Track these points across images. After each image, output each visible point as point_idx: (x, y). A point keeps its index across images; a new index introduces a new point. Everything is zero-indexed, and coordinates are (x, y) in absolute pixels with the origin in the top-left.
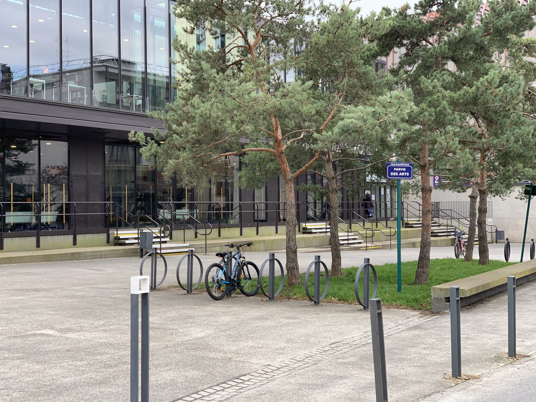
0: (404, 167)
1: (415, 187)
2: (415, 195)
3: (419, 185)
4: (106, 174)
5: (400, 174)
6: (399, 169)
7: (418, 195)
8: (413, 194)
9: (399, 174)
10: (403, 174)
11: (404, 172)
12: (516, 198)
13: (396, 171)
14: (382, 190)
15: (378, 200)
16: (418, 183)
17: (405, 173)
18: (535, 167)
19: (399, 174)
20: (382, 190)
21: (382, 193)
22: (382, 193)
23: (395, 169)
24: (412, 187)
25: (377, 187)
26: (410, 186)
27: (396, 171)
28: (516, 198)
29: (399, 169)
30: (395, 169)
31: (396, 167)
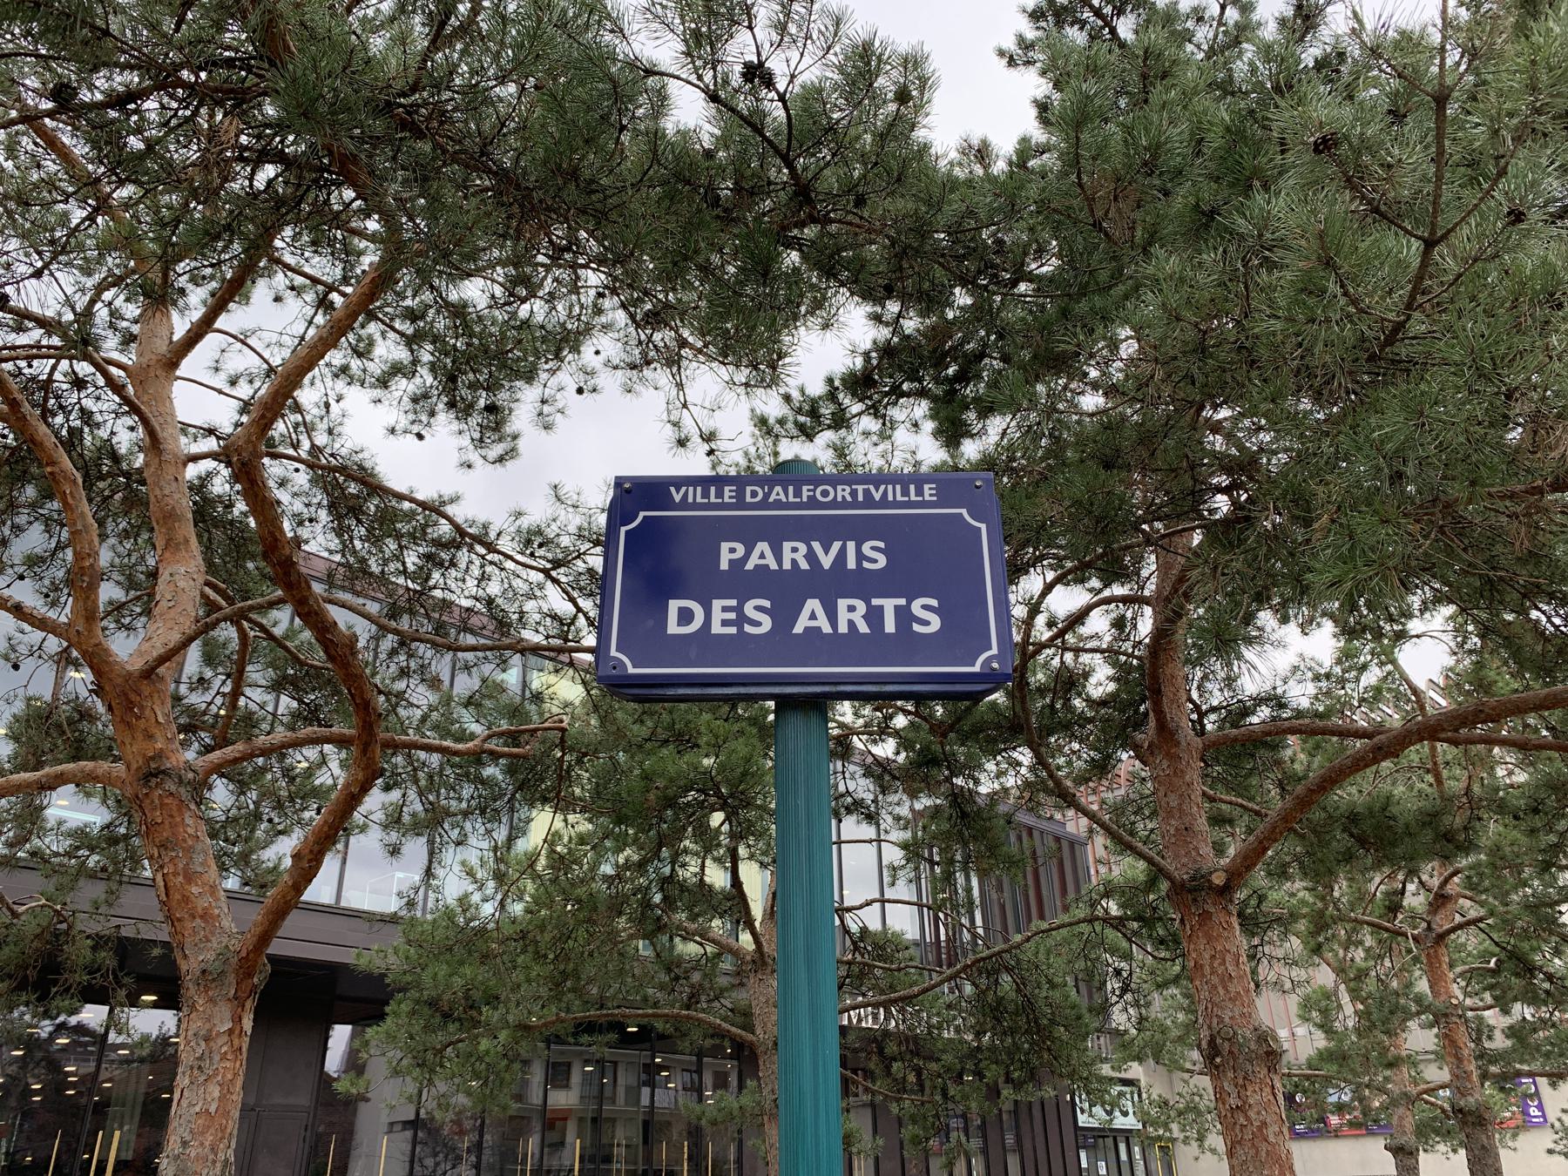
0: (859, 530)
1: (1191, 1116)
2: (1195, 1144)
3: (1202, 1107)
4: (856, 1164)
5: (811, 617)
6: (794, 554)
7: (1206, 1144)
8: (1186, 1141)
9: (784, 614)
10: (851, 613)
11: (863, 585)
12: (1550, 1152)
13: (742, 584)
14: (1122, 1147)
15: (1070, 1154)
16: (1197, 1099)
17: (889, 605)
18: (1561, 1076)
19: (784, 614)
20: (1122, 1147)
21: (1124, 1156)
22: (1124, 1156)
23: (728, 553)
24: (1180, 1114)
25: (1110, 1141)
26: (1173, 1114)
27: (742, 584)
28: (1550, 1152)
29: (794, 554)
30: (728, 553)
31: (749, 533)
